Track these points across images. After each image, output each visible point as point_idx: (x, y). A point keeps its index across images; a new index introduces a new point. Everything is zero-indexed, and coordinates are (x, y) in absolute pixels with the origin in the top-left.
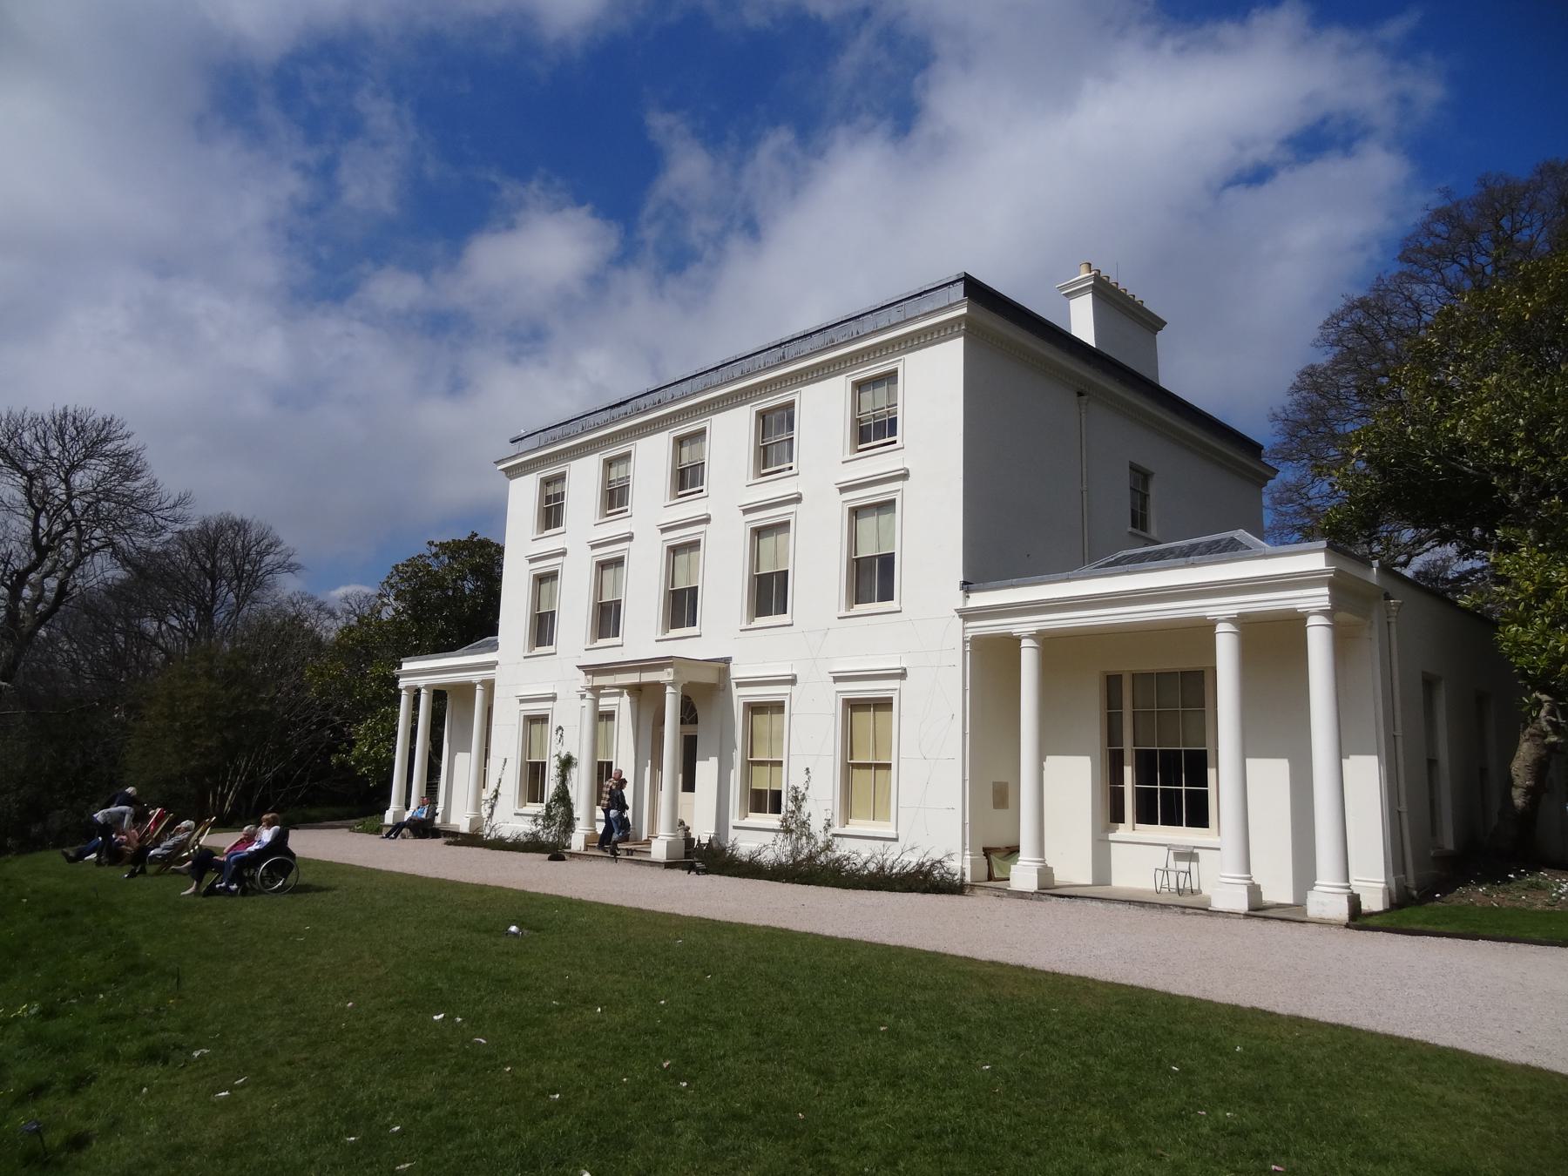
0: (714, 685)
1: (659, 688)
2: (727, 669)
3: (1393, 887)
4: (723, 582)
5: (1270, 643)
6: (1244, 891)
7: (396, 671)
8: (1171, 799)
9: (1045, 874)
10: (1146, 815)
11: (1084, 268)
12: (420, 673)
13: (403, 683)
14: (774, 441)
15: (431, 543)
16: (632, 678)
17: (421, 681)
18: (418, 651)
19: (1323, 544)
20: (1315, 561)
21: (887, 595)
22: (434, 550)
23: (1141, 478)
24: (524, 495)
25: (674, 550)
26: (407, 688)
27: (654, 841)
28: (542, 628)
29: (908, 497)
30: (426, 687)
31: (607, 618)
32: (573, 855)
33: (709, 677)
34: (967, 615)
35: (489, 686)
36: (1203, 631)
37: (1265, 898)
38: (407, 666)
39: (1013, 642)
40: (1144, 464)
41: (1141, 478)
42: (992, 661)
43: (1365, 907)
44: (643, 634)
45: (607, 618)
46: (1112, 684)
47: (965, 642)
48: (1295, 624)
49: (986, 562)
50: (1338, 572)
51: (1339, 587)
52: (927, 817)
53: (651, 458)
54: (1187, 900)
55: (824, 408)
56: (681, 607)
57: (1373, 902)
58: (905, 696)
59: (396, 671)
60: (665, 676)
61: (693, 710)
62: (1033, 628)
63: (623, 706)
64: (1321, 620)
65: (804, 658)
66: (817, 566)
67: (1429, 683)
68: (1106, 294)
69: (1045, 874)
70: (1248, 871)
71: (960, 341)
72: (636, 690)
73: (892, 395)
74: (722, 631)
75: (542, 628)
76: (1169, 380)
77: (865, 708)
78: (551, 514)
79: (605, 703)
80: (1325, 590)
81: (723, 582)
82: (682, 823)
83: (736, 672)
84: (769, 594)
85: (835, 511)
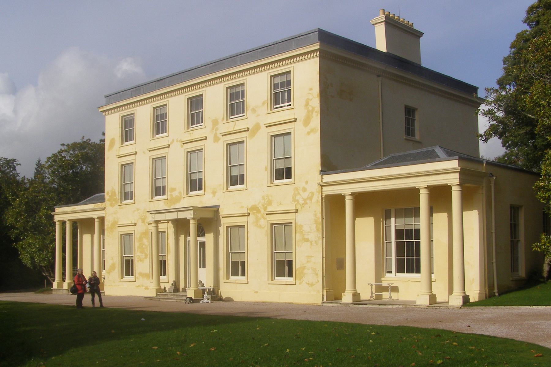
0: (212, 218)
3: (487, 292)
4: (214, 173)
5: (440, 196)
6: (427, 297)
7: (52, 213)
9: (356, 295)
11: (381, 12)
12: (64, 214)
13: (57, 218)
15: (63, 145)
16: (174, 216)
17: (66, 218)
19: (457, 157)
20: (454, 164)
22: (66, 147)
23: (410, 112)
24: (112, 126)
26: (59, 221)
27: (187, 290)
30: (69, 220)
32: (322, 179)
36: (414, 192)
37: (437, 300)
38: (58, 210)
39: (65, 222)
40: (411, 104)
41: (410, 112)
42: (333, 205)
43: (438, 300)
47: (322, 199)
51: (463, 173)
52: (302, 293)
54: (379, 301)
56: (195, 184)
57: (474, 297)
59: (52, 213)
60: (189, 215)
61: (203, 230)
63: (170, 229)
67: (514, 210)
68: (393, 25)
69: (356, 295)
70: (431, 290)
71: (317, 59)
76: (427, 62)
78: (127, 134)
79: (162, 227)
80: (458, 174)
81: (214, 173)
82: (201, 282)
83: (223, 212)
85: (264, 136)
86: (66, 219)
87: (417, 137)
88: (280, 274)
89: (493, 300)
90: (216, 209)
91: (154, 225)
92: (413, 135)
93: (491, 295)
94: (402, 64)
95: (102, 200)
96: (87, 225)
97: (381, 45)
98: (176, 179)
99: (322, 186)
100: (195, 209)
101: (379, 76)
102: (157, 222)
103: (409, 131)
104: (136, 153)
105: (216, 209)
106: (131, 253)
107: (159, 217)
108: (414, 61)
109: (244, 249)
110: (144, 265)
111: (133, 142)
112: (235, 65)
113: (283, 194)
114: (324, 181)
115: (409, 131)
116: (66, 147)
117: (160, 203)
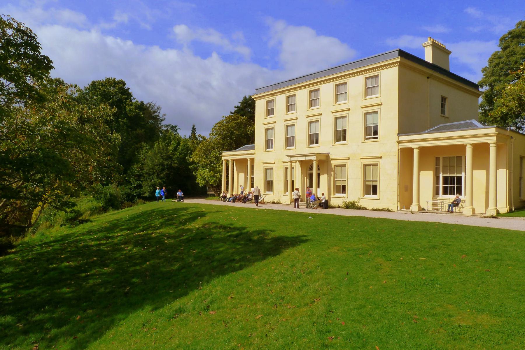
1: (311, 161)
2: (329, 156)
4: (326, 134)
5: (481, 150)
8: (452, 189)
10: (445, 192)
12: (228, 156)
14: (339, 93)
17: (229, 158)
18: (227, 150)
19: (495, 126)
20: (492, 130)
21: (345, 139)
23: (443, 99)
25: (267, 130)
28: (269, 144)
29: (382, 110)
31: (290, 141)
33: (323, 158)
34: (399, 142)
35: (252, 160)
36: (463, 147)
39: (411, 150)
40: (445, 95)
41: (443, 99)
42: (406, 155)
44: (302, 147)
45: (290, 141)
46: (437, 159)
48: (486, 146)
49: (405, 128)
50: (499, 133)
53: (302, 96)
55: (327, 90)
56: (314, 139)
58: (382, 162)
60: (313, 158)
62: (418, 146)
63: (298, 167)
64: (417, 150)
65: (352, 153)
66: (355, 127)
72: (301, 162)
73: (377, 82)
74: (327, 145)
75: (269, 144)
77: (369, 167)
80: (495, 137)
81: (326, 134)
83: (331, 157)
84: (341, 136)
86: (415, 146)
87: (447, 114)
88: (368, 193)
89: (511, 214)
90: (327, 155)
91: (289, 163)
92: (444, 114)
93: (510, 211)
94: (439, 71)
95: (253, 148)
96: (242, 163)
97: (429, 58)
98: (301, 136)
99: (399, 143)
100: (317, 155)
101: (428, 78)
102: (291, 162)
103: (443, 112)
104: (275, 123)
105: (327, 155)
106: (271, 178)
107: (292, 159)
108: (446, 69)
109: (345, 178)
110: (279, 185)
111: (273, 116)
112: (288, 86)
113: (372, 148)
114: (400, 140)
115: (443, 112)
116: (225, 118)
117: (291, 151)
